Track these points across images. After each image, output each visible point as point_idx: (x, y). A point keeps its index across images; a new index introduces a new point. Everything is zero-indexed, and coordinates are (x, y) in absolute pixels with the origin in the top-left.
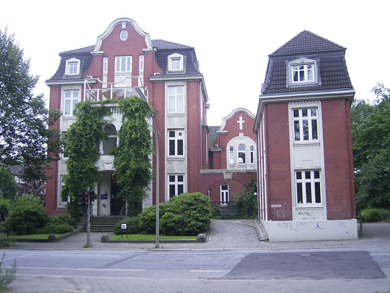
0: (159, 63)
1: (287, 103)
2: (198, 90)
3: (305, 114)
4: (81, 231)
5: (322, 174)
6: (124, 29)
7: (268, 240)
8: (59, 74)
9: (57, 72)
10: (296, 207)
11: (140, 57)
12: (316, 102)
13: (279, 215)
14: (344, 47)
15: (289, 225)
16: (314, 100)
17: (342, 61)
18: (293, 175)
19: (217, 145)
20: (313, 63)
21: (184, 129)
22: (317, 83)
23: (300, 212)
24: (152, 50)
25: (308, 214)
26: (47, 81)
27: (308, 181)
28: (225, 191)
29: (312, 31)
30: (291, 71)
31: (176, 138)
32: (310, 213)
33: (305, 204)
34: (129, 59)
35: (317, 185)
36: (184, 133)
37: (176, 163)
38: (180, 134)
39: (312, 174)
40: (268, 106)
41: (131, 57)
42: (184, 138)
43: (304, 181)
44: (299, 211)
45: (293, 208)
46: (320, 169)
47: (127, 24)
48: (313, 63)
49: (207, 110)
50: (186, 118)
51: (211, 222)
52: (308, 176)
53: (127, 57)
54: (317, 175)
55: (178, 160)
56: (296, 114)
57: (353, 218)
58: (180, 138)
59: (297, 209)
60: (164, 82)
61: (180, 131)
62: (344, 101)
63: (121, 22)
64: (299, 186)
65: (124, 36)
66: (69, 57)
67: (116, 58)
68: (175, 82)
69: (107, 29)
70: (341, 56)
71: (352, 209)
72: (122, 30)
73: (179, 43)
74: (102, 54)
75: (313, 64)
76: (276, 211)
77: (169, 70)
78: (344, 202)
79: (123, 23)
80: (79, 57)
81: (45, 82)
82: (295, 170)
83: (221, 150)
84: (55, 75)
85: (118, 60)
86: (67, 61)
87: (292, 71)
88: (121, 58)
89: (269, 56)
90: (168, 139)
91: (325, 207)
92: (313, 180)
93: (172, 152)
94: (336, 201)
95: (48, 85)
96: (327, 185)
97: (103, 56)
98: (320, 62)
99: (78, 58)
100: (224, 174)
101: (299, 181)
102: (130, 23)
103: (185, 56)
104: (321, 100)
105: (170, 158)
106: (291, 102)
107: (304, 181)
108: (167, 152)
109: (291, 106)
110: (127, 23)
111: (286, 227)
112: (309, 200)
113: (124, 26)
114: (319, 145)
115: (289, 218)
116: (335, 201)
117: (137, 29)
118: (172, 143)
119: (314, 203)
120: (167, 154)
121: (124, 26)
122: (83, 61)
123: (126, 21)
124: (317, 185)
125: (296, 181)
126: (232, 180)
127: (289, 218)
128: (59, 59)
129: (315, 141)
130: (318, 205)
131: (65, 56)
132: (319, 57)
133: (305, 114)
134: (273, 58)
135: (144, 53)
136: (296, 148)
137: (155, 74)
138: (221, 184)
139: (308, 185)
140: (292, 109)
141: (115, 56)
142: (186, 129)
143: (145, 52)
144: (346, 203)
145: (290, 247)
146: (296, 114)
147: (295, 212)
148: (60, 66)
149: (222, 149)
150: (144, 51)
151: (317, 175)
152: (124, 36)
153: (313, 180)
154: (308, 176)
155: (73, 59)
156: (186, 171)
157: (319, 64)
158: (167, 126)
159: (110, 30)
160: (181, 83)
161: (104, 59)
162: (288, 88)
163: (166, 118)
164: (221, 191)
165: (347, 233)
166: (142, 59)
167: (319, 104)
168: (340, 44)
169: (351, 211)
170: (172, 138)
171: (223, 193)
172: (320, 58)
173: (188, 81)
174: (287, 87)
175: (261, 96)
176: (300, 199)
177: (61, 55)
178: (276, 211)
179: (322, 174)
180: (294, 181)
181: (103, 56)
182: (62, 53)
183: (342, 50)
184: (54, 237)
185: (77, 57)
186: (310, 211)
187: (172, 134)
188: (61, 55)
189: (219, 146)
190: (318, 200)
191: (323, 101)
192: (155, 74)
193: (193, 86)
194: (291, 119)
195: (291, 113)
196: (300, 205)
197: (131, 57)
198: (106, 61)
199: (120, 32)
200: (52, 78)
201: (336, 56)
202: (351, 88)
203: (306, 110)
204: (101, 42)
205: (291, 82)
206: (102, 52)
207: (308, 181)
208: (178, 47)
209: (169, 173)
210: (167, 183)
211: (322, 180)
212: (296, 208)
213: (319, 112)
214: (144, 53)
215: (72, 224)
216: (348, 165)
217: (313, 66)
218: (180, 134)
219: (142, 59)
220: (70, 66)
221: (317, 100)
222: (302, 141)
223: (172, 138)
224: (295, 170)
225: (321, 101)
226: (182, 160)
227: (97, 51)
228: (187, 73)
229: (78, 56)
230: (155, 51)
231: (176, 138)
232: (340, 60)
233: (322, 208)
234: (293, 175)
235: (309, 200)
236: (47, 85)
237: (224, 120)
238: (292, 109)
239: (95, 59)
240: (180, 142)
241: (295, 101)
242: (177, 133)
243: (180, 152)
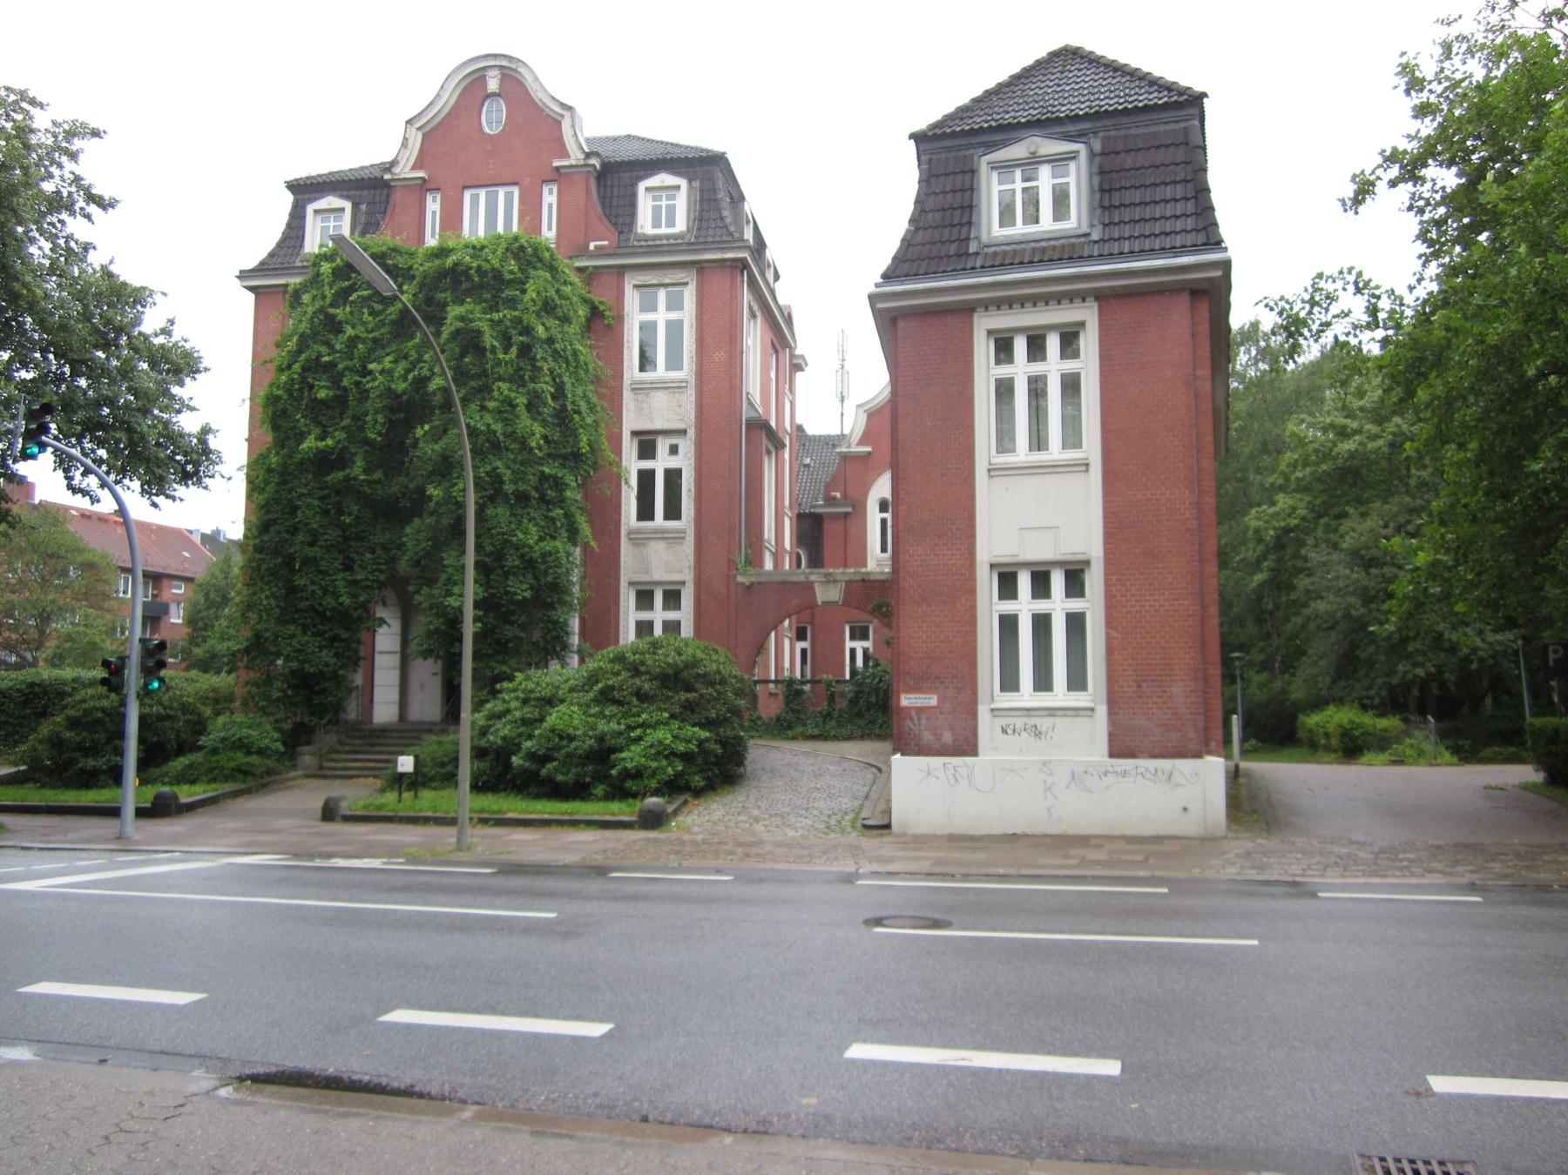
0: (607, 211)
1: (966, 311)
2: (734, 300)
3: (1036, 348)
4: (307, 776)
5: (1094, 581)
6: (494, 95)
7: (888, 826)
8: (283, 252)
9: (280, 245)
10: (994, 706)
11: (546, 189)
12: (1077, 303)
13: (927, 737)
14: (1198, 87)
15: (963, 772)
16: (1071, 297)
17: (1187, 144)
18: (987, 584)
19: (838, 495)
20: (1073, 156)
21: (683, 432)
22: (1088, 230)
23: (1008, 725)
24: (582, 162)
25: (1037, 733)
26: (243, 275)
27: (1042, 606)
28: (859, 645)
29: (1088, 47)
30: (993, 189)
31: (661, 463)
32: (1044, 729)
33: (1027, 695)
34: (509, 197)
35: (1076, 623)
36: (687, 446)
37: (657, 549)
38: (674, 450)
39: (1058, 581)
40: (901, 324)
41: (516, 191)
42: (684, 461)
43: (1025, 606)
44: (1004, 722)
45: (983, 711)
46: (1087, 563)
47: (503, 75)
48: (1073, 156)
49: (799, 375)
50: (690, 396)
51: (412, 793)
52: (1041, 585)
53: (501, 192)
54: (1075, 583)
55: (661, 535)
56: (1004, 349)
57: (1210, 753)
58: (673, 463)
59: (996, 713)
60: (621, 270)
61: (674, 441)
62: (1186, 297)
63: (484, 69)
64: (1008, 625)
65: (493, 119)
66: (313, 196)
67: (467, 195)
68: (661, 273)
69: (438, 95)
70: (1182, 125)
71: (1206, 716)
72: (489, 96)
73: (681, 143)
74: (419, 182)
75: (1074, 158)
76: (919, 719)
77: (639, 231)
78: (1177, 689)
79: (491, 73)
80: (351, 193)
81: (94, 248)
82: (992, 566)
83: (850, 510)
84: (272, 255)
85: (475, 201)
86: (310, 209)
87: (996, 188)
88: (482, 193)
89: (913, 136)
90: (633, 464)
91: (1102, 711)
92: (1058, 605)
93: (646, 512)
94: (1144, 684)
95: (251, 289)
96: (1110, 622)
97: (424, 187)
98: (1101, 154)
99: (347, 198)
100: (816, 585)
101: (1008, 607)
102: (512, 73)
103: (696, 184)
104: (1101, 297)
105: (638, 531)
106: (986, 305)
107: (1025, 606)
108: (628, 511)
109: (983, 324)
110: (506, 71)
111: (952, 781)
112: (1043, 681)
113: (493, 85)
114: (1087, 471)
115: (966, 746)
116: (1139, 686)
117: (538, 96)
118: (646, 478)
119: (1060, 695)
120: (628, 517)
121: (493, 85)
122: (363, 207)
123: (501, 67)
124: (1076, 623)
125: (996, 608)
126: (843, 604)
127: (966, 746)
128: (288, 198)
129: (1072, 455)
130: (1079, 699)
131: (305, 190)
132: (1101, 134)
133: (1036, 348)
134: (928, 146)
135: (558, 175)
136: (999, 483)
137: (592, 246)
138: (848, 622)
139: (1042, 624)
140: (990, 332)
141: (465, 187)
142: (691, 433)
143: (562, 171)
144: (1181, 692)
145: (940, 862)
146: (1004, 349)
147: (987, 726)
148: (289, 226)
149: (854, 507)
150: (557, 169)
151: (1075, 583)
152: (493, 119)
153: (1058, 605)
154: (1041, 585)
155: (331, 201)
156: (688, 576)
157: (1098, 160)
158: (632, 420)
159: (449, 98)
160: (680, 276)
161: (429, 198)
162: (977, 254)
163: (627, 395)
164: (849, 644)
165: (1185, 809)
166: (550, 197)
167: (1088, 314)
168: (1184, 82)
169: (1201, 725)
170: (647, 464)
171: (853, 651)
172: (1104, 137)
173: (700, 267)
174: (971, 251)
175: (877, 285)
176: (1010, 682)
177: (296, 187)
178: (919, 719)
179: (1094, 581)
180: (989, 606)
181: (424, 187)
182: (296, 180)
183: (1191, 103)
184: (175, 797)
185: (345, 193)
186: (1044, 723)
187: (647, 449)
188: (296, 187)
189: (845, 496)
190: (1077, 681)
191: (1107, 298)
192: (592, 246)
193: (719, 281)
194: (985, 370)
195: (983, 350)
196: (1007, 700)
197: (516, 191)
198: (433, 205)
199: (483, 105)
200: (262, 263)
201: (1163, 127)
202: (1216, 243)
203: (1043, 338)
204: (416, 140)
205: (993, 229)
206: (421, 174)
207: (1042, 606)
208: (676, 153)
209: (633, 580)
210: (627, 614)
211: (1092, 605)
212: (993, 710)
213: (1089, 342)
214: (558, 175)
215: (281, 756)
216: (1196, 548)
217: (1072, 165)
218: (674, 450)
219: (550, 197)
220: (319, 224)
221: (1083, 296)
222: (1022, 452)
223: (647, 464)
224: (992, 566)
225: (1097, 299)
226: (675, 538)
227: (405, 171)
228: (701, 240)
229: (350, 189)
230: (594, 166)
231: (661, 463)
232: (1182, 139)
233: (1089, 713)
234: (987, 584)
235: (1043, 681)
236: (246, 287)
237: (861, 412)
238: (990, 332)
239: (397, 196)
240: (673, 477)
241: (999, 304)
242: (662, 446)
243: (673, 512)
